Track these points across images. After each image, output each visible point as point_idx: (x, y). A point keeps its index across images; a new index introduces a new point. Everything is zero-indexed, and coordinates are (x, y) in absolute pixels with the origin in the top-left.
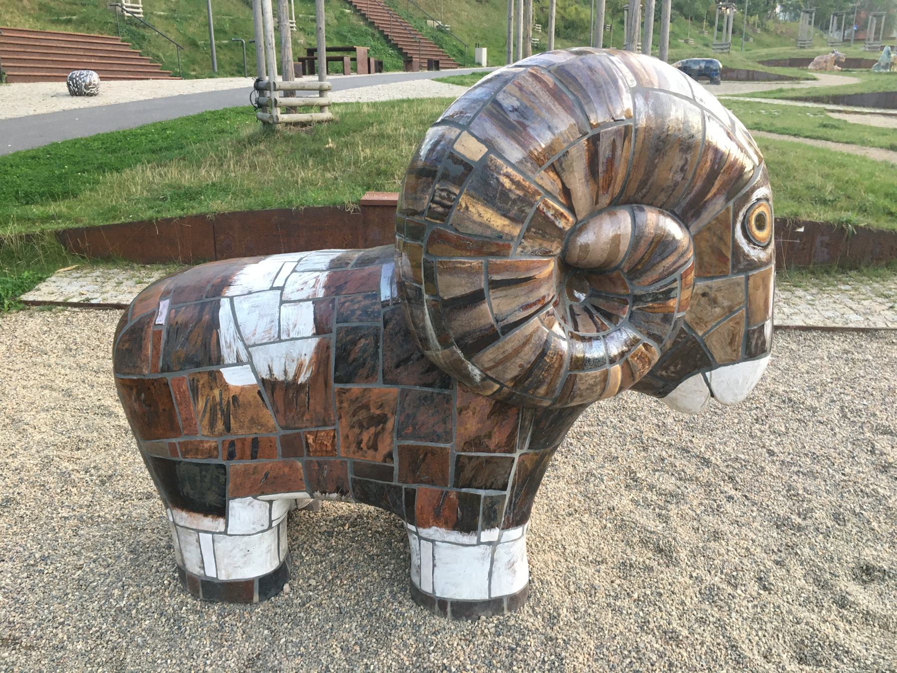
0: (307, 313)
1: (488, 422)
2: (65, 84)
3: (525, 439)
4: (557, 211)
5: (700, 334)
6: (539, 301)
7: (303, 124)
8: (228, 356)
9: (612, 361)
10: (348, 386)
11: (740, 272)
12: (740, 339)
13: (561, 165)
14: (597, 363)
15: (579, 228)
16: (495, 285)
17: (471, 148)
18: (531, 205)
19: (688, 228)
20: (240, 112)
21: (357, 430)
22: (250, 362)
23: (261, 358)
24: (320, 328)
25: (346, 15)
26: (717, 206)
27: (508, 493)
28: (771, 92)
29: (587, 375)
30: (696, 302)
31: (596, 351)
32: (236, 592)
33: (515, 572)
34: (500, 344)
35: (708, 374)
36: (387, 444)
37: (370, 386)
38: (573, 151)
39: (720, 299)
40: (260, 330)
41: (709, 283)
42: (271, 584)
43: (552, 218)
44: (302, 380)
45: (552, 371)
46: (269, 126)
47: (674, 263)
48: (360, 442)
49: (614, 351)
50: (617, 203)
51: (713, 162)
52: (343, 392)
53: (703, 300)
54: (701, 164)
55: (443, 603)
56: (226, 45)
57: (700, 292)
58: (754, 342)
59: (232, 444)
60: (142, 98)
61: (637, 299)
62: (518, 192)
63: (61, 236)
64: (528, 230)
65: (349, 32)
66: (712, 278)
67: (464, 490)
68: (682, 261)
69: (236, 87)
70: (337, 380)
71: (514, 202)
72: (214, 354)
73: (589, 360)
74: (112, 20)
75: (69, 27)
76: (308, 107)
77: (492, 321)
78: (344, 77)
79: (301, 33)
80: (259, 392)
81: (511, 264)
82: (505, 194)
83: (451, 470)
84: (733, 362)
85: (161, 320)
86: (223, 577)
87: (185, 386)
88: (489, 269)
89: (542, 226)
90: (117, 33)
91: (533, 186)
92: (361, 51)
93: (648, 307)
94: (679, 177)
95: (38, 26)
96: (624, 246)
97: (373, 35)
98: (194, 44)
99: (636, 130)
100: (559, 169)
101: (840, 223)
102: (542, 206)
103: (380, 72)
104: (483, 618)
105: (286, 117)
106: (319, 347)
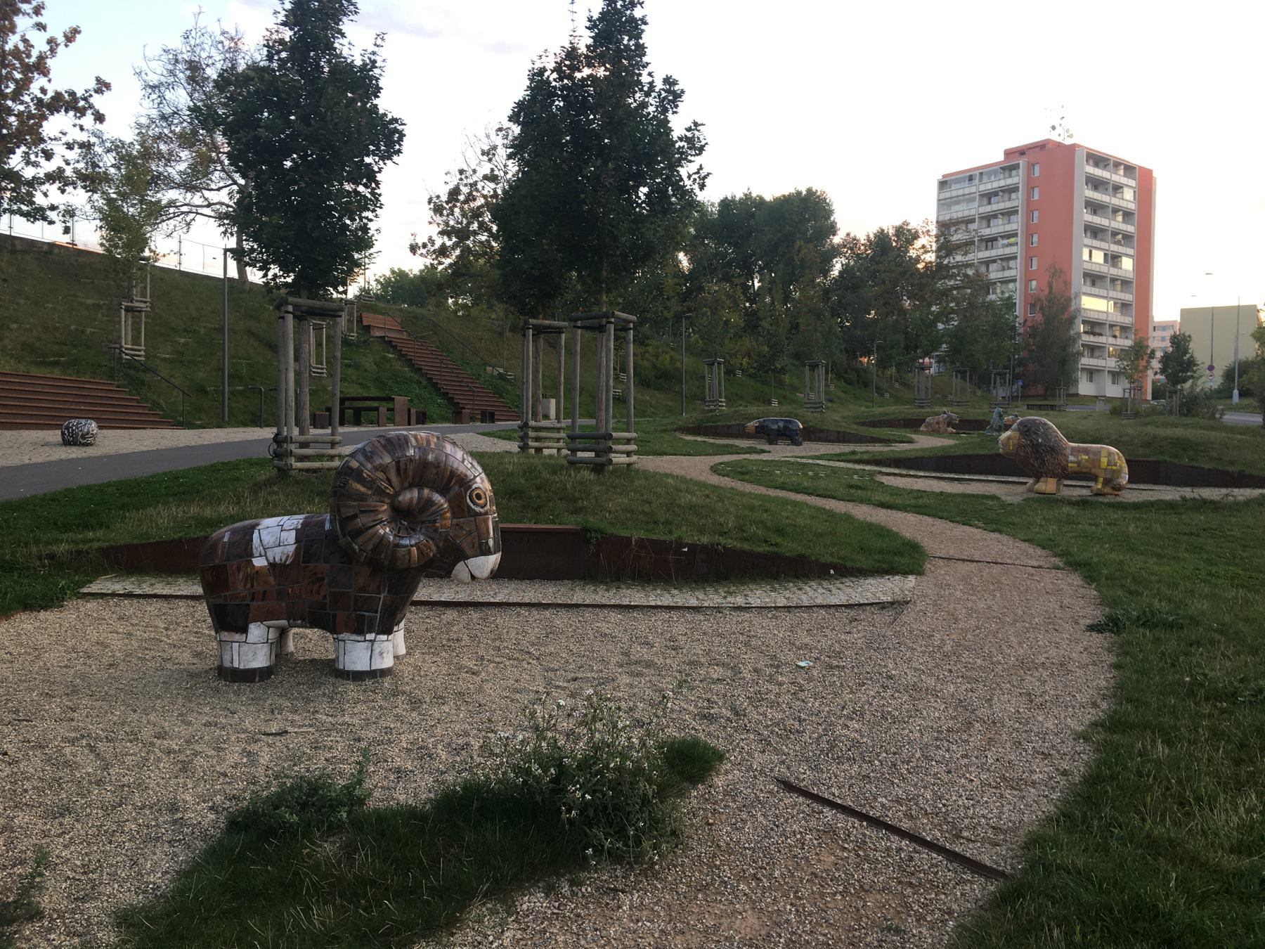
0: (293, 533)
2: (59, 432)
7: (315, 471)
8: (256, 553)
12: (477, 545)
15: (397, 494)
16: (362, 512)
17: (354, 464)
20: (260, 463)
23: (270, 554)
24: (298, 540)
25: (389, 360)
28: (844, 454)
31: (406, 542)
32: (247, 676)
46: (284, 473)
49: (413, 542)
50: (411, 486)
56: (240, 392)
60: (144, 449)
61: (423, 522)
63: (105, 552)
69: (250, 438)
76: (319, 457)
78: (355, 429)
85: (225, 540)
89: (380, 492)
90: (112, 377)
92: (400, 401)
95: (22, 368)
96: (415, 501)
98: (202, 390)
101: (712, 545)
105: (299, 465)
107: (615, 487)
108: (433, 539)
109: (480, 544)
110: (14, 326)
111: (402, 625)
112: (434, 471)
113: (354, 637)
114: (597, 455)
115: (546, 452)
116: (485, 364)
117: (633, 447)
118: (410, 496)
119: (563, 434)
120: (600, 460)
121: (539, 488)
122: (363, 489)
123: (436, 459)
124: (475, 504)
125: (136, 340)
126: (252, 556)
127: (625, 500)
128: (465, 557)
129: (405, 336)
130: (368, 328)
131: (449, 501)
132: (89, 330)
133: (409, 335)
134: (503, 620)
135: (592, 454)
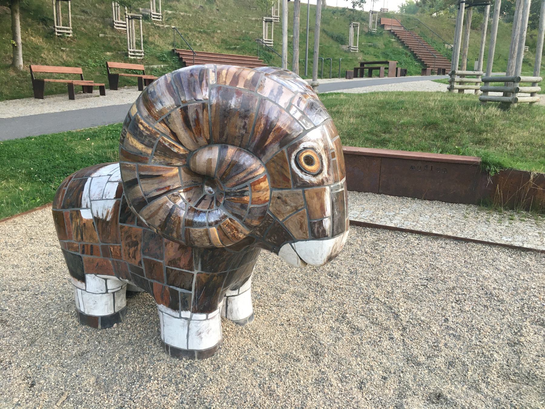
1: (179, 252)
3: (198, 264)
4: (170, 143)
5: (281, 220)
6: (166, 187)
8: (84, 206)
9: (210, 225)
10: (124, 225)
11: (298, 187)
13: (167, 120)
14: (201, 225)
16: (142, 177)
18: (155, 139)
19: (260, 159)
21: (128, 248)
22: (91, 208)
25: (391, 42)
26: (274, 150)
27: (193, 292)
29: (195, 230)
30: (275, 202)
33: (201, 338)
34: (147, 207)
35: (293, 244)
36: (140, 256)
37: (131, 226)
38: (173, 114)
39: (288, 201)
40: (97, 193)
41: (280, 191)
42: (107, 322)
43: (169, 147)
44: (108, 219)
45: (176, 225)
47: (245, 177)
48: (129, 254)
49: (212, 220)
50: (210, 143)
51: (266, 125)
52: (122, 227)
53: (279, 201)
54: (257, 125)
55: (167, 346)
57: (276, 196)
58: (316, 230)
59: (83, 246)
62: (147, 132)
64: (156, 151)
65: (392, 52)
66: (282, 189)
67: (171, 287)
68: (250, 176)
70: (120, 222)
71: (146, 137)
72: (79, 203)
73: (196, 222)
74: (256, 48)
75: (234, 52)
77: (142, 194)
79: (361, 54)
80: (93, 223)
81: (148, 167)
82: (141, 133)
83: (165, 275)
84: (306, 239)
86: (86, 313)
87: (69, 216)
88: (140, 169)
89: (165, 151)
91: (154, 130)
92: (393, 63)
93: (232, 199)
94: (243, 132)
95: (218, 51)
96: (214, 165)
97: (406, 54)
99: (211, 106)
100: (167, 122)
102: (161, 140)
103: (405, 76)
104: (184, 359)
106: (116, 203)
107: (518, 122)
108: (239, 217)
109: (311, 225)
110: (219, 31)
111: (248, 284)
112: (240, 123)
113: (170, 311)
114: (505, 95)
115: (466, 92)
116: (444, 43)
117: (537, 88)
118: (209, 156)
119: (480, 79)
120: (507, 99)
121: (451, 121)
122: (140, 146)
123: (242, 104)
124: (306, 172)
125: (270, 37)
126: (79, 206)
127: (526, 134)
128: (289, 239)
129: (402, 29)
130: (383, 26)
131: (266, 166)
132: (251, 32)
133: (405, 29)
134: (393, 248)
135: (501, 94)
